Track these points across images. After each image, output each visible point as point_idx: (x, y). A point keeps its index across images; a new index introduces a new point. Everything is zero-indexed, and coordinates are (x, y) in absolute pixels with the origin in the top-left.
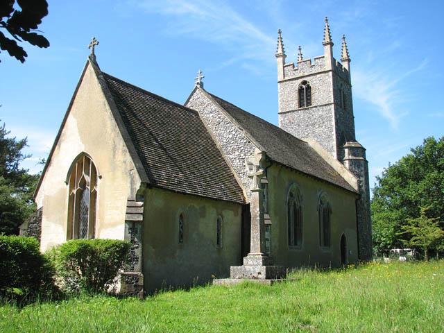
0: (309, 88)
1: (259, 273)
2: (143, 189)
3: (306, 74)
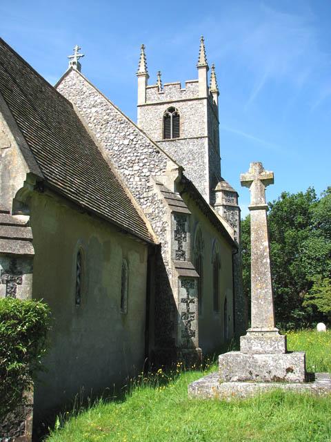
0: (177, 116)
1: (289, 370)
2: (30, 189)
3: (174, 99)
